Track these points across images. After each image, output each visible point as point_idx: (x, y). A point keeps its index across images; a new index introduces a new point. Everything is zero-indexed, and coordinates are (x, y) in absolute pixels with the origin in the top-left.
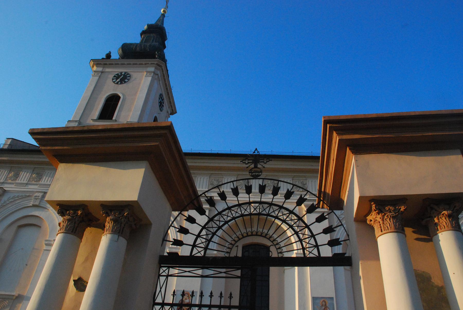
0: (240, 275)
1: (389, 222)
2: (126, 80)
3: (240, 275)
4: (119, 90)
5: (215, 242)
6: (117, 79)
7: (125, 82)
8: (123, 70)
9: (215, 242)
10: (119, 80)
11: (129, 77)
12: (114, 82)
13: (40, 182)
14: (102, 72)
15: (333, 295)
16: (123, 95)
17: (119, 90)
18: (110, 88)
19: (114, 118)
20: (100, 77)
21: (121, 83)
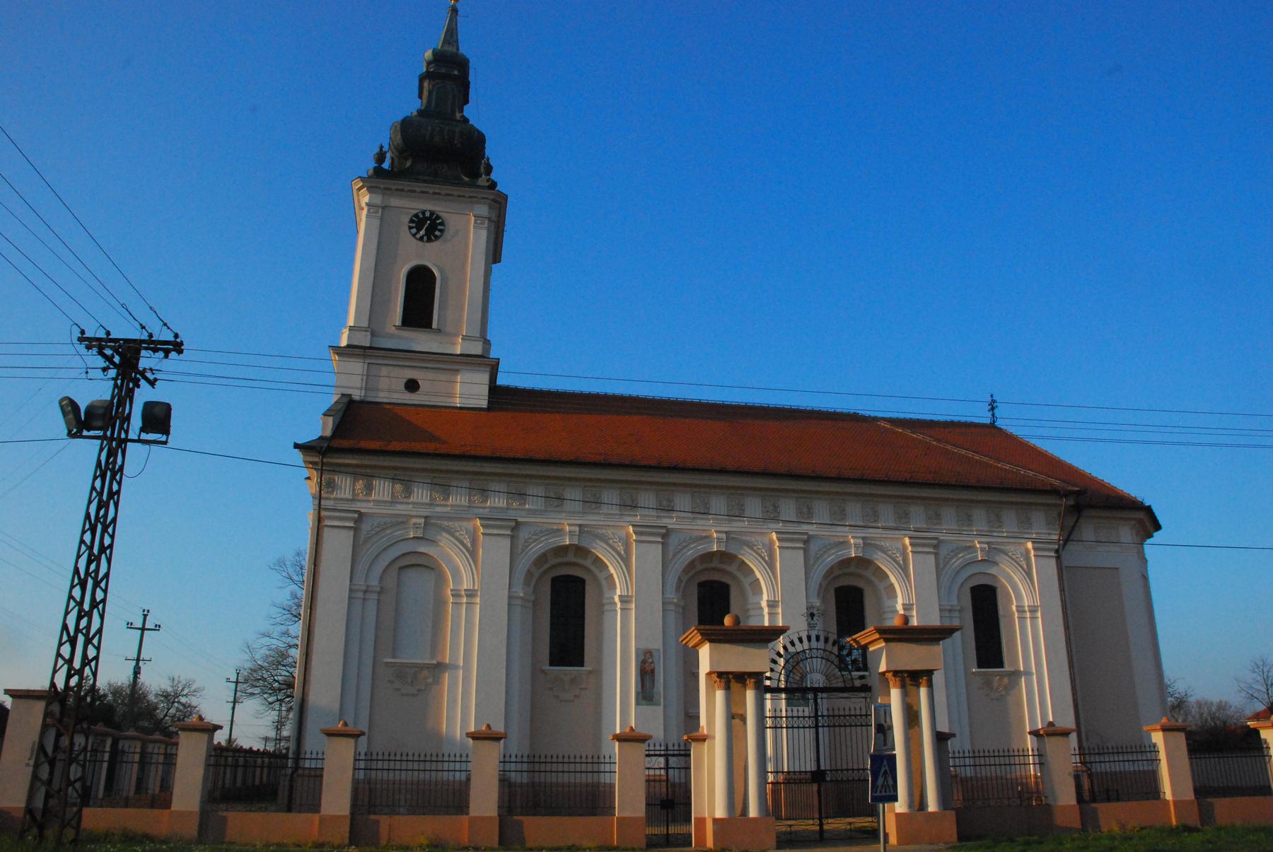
0: (499, 383)
1: (898, 683)
2: (437, 233)
3: (499, 383)
4: (429, 255)
5: (91, 578)
6: (419, 231)
7: (437, 238)
8: (428, 206)
9: (91, 578)
10: (422, 232)
11: (441, 231)
12: (414, 235)
13: (334, 495)
14: (383, 208)
15: (661, 647)
16: (441, 271)
17: (429, 255)
18: (413, 253)
19: (434, 325)
20: (381, 219)
21: (429, 240)
